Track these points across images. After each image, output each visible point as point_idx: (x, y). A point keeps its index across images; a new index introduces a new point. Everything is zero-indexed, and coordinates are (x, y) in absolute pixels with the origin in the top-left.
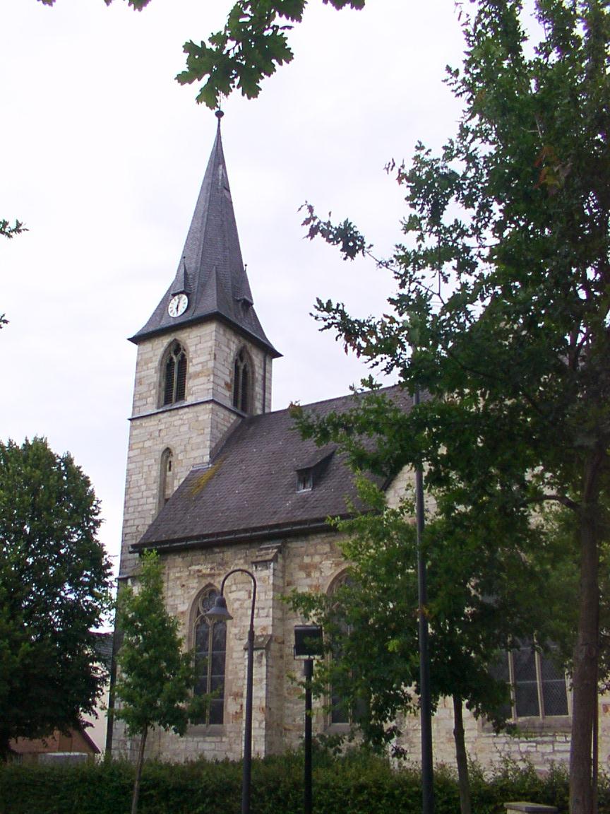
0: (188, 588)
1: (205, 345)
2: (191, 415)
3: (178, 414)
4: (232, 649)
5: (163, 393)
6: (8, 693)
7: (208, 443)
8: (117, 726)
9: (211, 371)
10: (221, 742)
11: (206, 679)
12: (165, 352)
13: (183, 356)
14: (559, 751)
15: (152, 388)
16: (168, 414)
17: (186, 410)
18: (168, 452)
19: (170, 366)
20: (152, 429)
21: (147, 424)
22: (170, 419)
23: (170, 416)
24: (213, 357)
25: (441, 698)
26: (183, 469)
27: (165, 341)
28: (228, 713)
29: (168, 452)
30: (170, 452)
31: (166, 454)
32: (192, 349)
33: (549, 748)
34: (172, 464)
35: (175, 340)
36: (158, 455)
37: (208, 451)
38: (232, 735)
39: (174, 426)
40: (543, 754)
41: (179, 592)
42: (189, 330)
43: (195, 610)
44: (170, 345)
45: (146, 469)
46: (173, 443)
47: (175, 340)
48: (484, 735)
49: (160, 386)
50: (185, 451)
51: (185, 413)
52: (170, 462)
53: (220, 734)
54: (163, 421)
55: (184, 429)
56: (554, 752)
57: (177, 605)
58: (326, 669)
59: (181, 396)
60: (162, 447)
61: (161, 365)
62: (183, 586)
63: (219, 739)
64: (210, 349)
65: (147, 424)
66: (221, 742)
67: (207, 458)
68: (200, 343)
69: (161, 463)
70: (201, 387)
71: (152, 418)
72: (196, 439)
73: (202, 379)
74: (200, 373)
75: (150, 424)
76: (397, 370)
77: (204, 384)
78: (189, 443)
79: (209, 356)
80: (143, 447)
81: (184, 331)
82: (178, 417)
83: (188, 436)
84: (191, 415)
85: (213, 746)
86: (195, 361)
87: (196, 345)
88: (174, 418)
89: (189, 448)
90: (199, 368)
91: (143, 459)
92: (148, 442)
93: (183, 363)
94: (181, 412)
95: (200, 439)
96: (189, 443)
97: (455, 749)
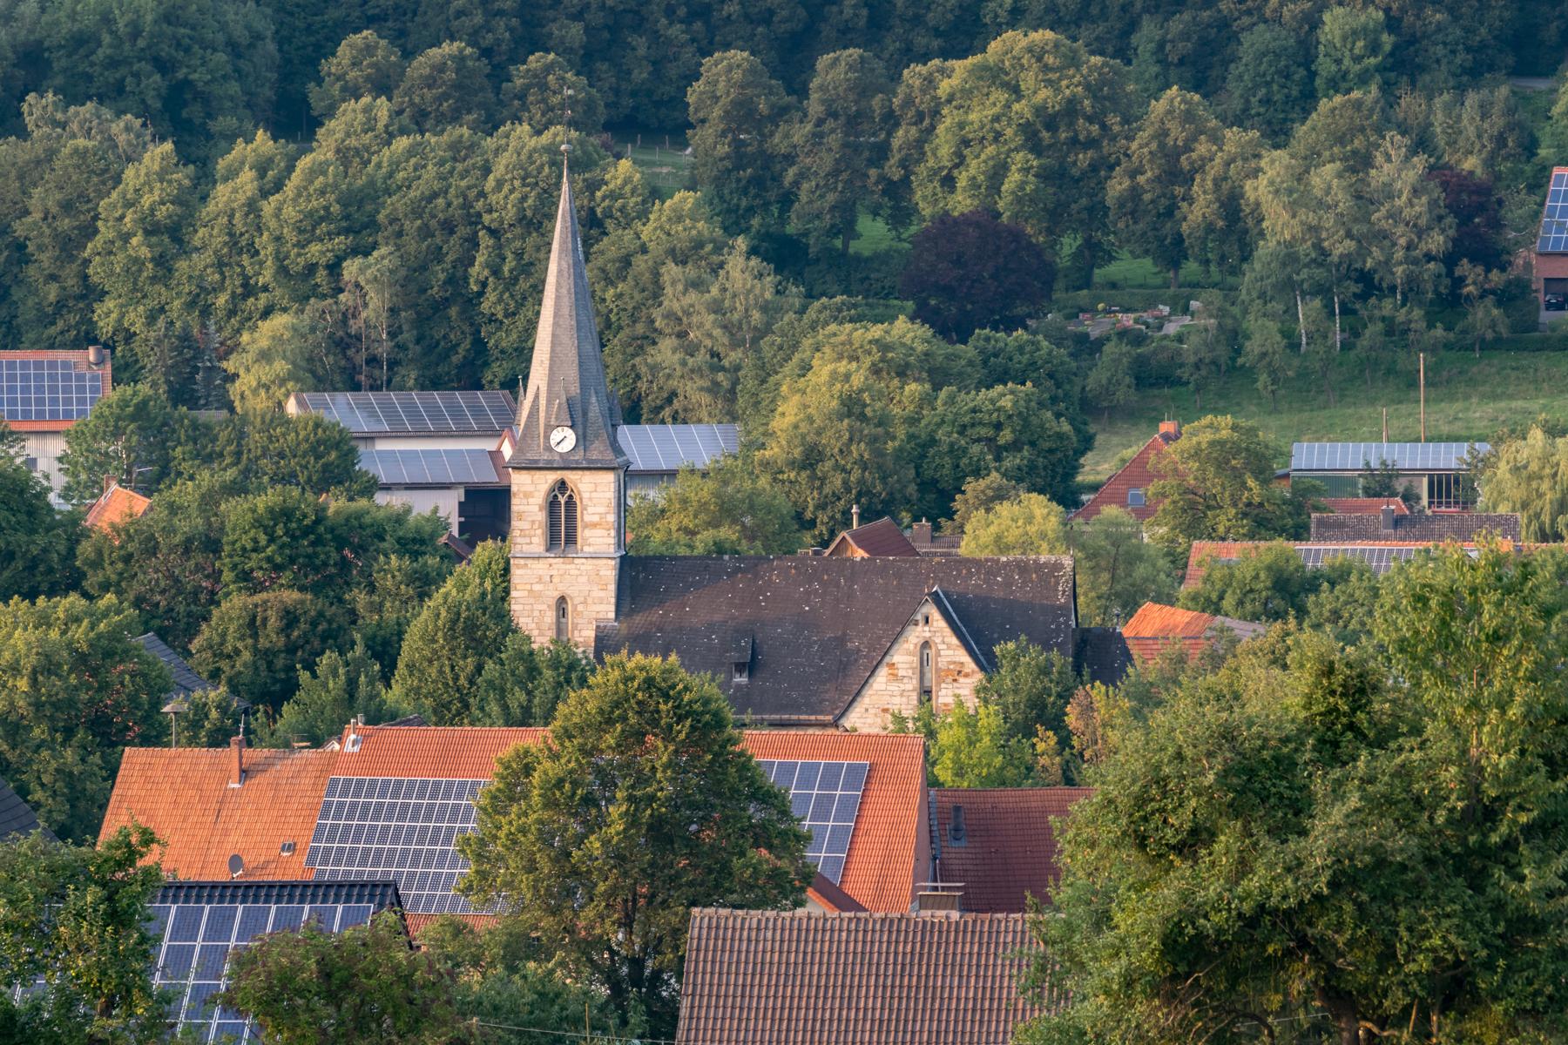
6: (531, 997)
11: (198, 976)
13: (570, 497)
18: (562, 601)
19: (552, 505)
27: (551, 477)
29: (562, 601)
32: (585, 495)
36: (553, 602)
45: (536, 613)
46: (563, 588)
55: (584, 579)
58: (735, 458)
59: (571, 539)
60: (557, 595)
72: (597, 593)
73: (599, 532)
76: (1350, 245)
86: (590, 510)
89: (590, 600)
90: (596, 519)
91: (268, 207)
95: (602, 594)
97: (514, 508)
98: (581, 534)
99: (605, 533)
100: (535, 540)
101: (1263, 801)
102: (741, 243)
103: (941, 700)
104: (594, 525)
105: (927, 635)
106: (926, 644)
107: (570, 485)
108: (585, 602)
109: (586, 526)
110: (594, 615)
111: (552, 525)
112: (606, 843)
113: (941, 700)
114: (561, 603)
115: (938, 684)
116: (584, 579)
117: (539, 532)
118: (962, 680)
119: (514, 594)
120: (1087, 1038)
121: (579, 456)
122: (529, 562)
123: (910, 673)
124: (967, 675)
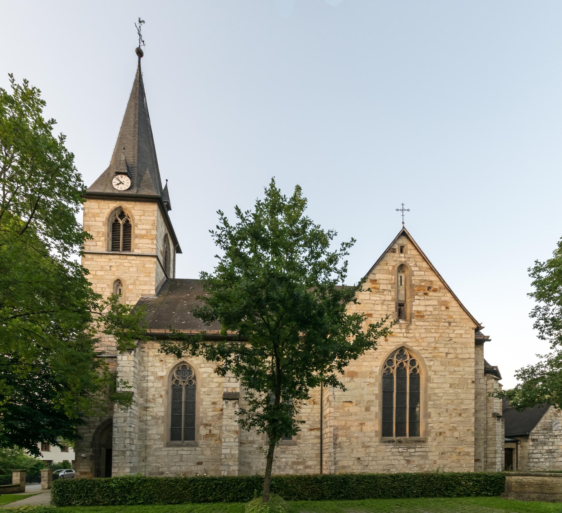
0: (166, 362)
1: (148, 218)
2: (138, 262)
3: (127, 259)
4: (202, 400)
5: (110, 242)
7: (154, 283)
8: (116, 443)
9: (154, 236)
10: (195, 450)
12: (112, 213)
13: (127, 221)
14: (417, 451)
15: (101, 235)
16: (118, 257)
17: (134, 257)
19: (115, 226)
20: (103, 264)
21: (97, 260)
22: (120, 261)
23: (119, 259)
24: (155, 228)
25: (162, 443)
26: (133, 295)
27: (112, 205)
28: (201, 435)
30: (120, 283)
31: (117, 283)
32: (137, 218)
33: (413, 450)
34: (121, 291)
35: (120, 207)
36: (111, 283)
37: (154, 288)
38: (203, 446)
39: (123, 266)
40: (410, 453)
41: (158, 364)
42: (133, 203)
43: (171, 377)
44: (116, 209)
46: (123, 277)
47: (120, 207)
48: (381, 444)
49: (108, 236)
50: (134, 284)
51: (133, 260)
52: (120, 290)
53: (197, 445)
54: (113, 260)
56: (415, 452)
57: (157, 372)
59: (127, 247)
60: (114, 278)
61: (108, 221)
62: (162, 361)
63: (194, 449)
64: (153, 222)
65: (97, 260)
66: (195, 450)
67: (153, 292)
68: (144, 215)
69: (113, 288)
70: (147, 245)
71: (103, 256)
72: (143, 278)
74: (145, 236)
75: (101, 260)
77: (148, 244)
78: (137, 280)
79: (152, 227)
80: (96, 274)
81: (129, 203)
82: (126, 261)
83: (136, 275)
84: (138, 262)
85: (189, 452)
86: (140, 227)
87: (140, 216)
88: (123, 261)
89: (137, 283)
90: (144, 232)
92: (100, 271)
93: (128, 227)
94: (129, 258)
95: (147, 279)
96: (137, 280)
98: (135, 241)
99: (150, 242)
100: (99, 244)
101: (221, 427)
102: (265, 406)
103: (414, 308)
104: (142, 237)
105: (403, 260)
106: (402, 267)
107: (126, 212)
108: (134, 284)
109: (136, 237)
110: (141, 292)
111: (113, 239)
112: (335, 281)
113: (414, 308)
114: (118, 282)
115: (412, 296)
116: (134, 269)
117: (103, 239)
118: (431, 294)
119: (375, 500)
120: (435, 465)
121: (134, 192)
122: (95, 257)
123: (389, 287)
124: (435, 290)
